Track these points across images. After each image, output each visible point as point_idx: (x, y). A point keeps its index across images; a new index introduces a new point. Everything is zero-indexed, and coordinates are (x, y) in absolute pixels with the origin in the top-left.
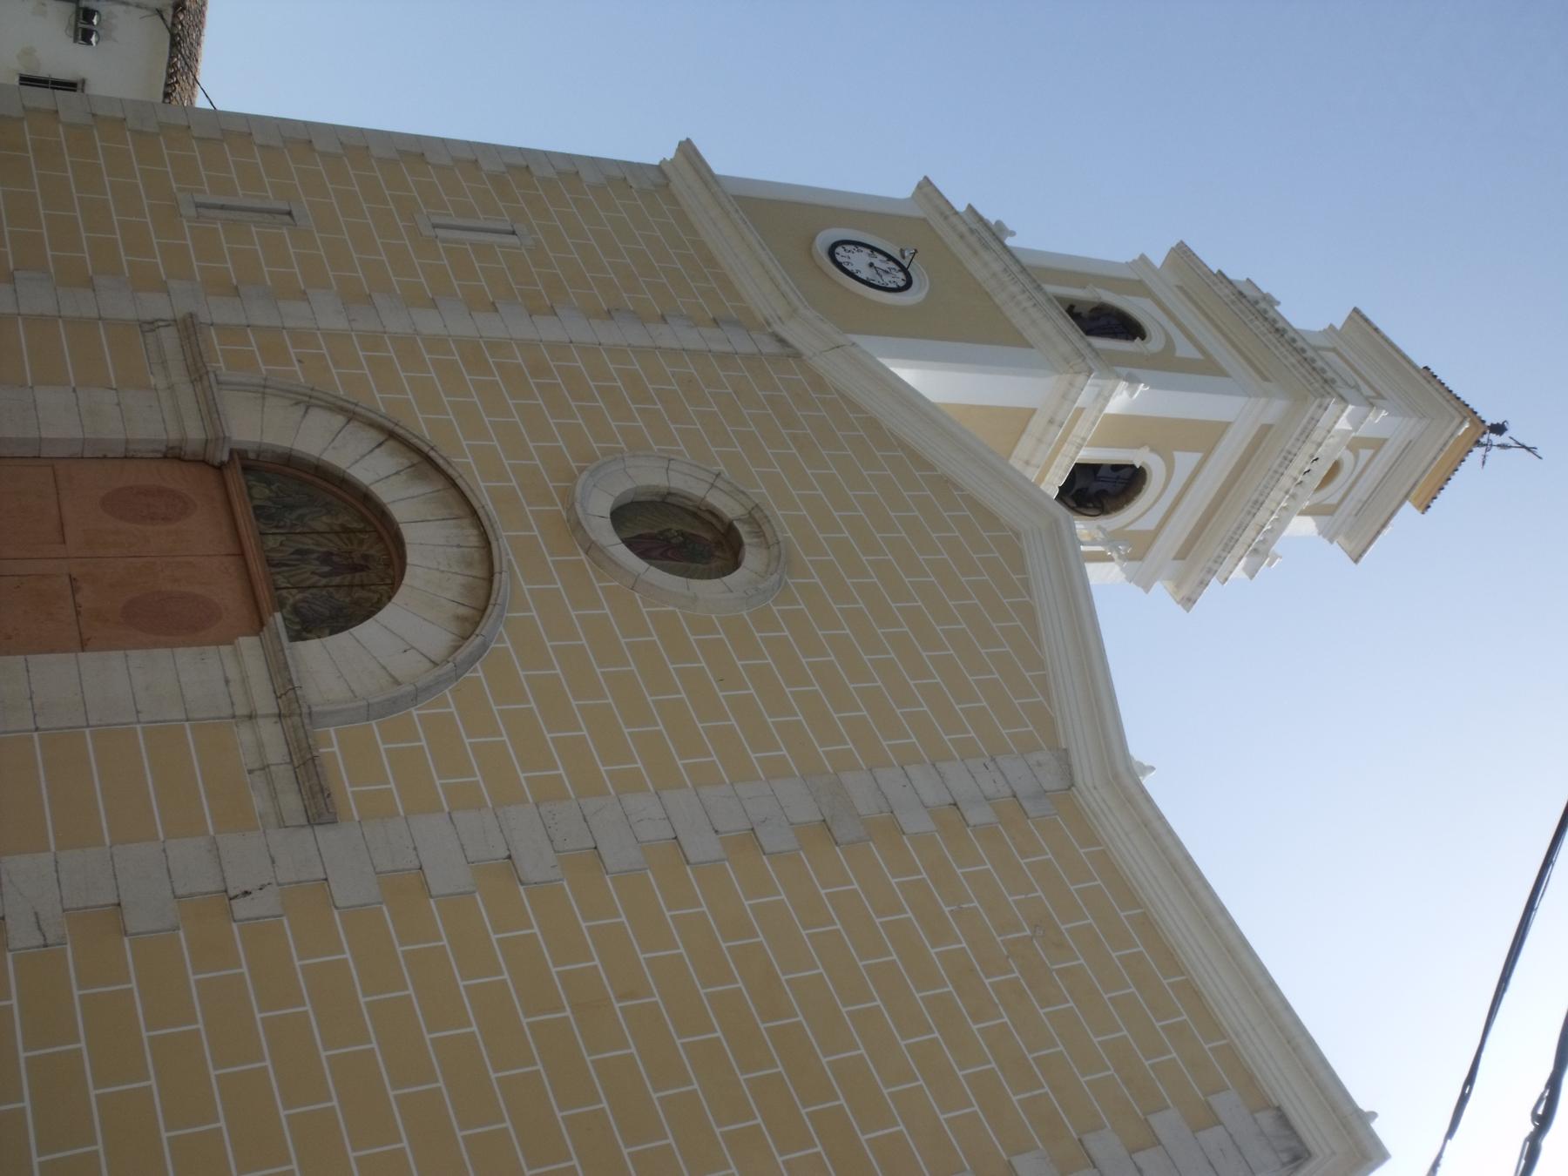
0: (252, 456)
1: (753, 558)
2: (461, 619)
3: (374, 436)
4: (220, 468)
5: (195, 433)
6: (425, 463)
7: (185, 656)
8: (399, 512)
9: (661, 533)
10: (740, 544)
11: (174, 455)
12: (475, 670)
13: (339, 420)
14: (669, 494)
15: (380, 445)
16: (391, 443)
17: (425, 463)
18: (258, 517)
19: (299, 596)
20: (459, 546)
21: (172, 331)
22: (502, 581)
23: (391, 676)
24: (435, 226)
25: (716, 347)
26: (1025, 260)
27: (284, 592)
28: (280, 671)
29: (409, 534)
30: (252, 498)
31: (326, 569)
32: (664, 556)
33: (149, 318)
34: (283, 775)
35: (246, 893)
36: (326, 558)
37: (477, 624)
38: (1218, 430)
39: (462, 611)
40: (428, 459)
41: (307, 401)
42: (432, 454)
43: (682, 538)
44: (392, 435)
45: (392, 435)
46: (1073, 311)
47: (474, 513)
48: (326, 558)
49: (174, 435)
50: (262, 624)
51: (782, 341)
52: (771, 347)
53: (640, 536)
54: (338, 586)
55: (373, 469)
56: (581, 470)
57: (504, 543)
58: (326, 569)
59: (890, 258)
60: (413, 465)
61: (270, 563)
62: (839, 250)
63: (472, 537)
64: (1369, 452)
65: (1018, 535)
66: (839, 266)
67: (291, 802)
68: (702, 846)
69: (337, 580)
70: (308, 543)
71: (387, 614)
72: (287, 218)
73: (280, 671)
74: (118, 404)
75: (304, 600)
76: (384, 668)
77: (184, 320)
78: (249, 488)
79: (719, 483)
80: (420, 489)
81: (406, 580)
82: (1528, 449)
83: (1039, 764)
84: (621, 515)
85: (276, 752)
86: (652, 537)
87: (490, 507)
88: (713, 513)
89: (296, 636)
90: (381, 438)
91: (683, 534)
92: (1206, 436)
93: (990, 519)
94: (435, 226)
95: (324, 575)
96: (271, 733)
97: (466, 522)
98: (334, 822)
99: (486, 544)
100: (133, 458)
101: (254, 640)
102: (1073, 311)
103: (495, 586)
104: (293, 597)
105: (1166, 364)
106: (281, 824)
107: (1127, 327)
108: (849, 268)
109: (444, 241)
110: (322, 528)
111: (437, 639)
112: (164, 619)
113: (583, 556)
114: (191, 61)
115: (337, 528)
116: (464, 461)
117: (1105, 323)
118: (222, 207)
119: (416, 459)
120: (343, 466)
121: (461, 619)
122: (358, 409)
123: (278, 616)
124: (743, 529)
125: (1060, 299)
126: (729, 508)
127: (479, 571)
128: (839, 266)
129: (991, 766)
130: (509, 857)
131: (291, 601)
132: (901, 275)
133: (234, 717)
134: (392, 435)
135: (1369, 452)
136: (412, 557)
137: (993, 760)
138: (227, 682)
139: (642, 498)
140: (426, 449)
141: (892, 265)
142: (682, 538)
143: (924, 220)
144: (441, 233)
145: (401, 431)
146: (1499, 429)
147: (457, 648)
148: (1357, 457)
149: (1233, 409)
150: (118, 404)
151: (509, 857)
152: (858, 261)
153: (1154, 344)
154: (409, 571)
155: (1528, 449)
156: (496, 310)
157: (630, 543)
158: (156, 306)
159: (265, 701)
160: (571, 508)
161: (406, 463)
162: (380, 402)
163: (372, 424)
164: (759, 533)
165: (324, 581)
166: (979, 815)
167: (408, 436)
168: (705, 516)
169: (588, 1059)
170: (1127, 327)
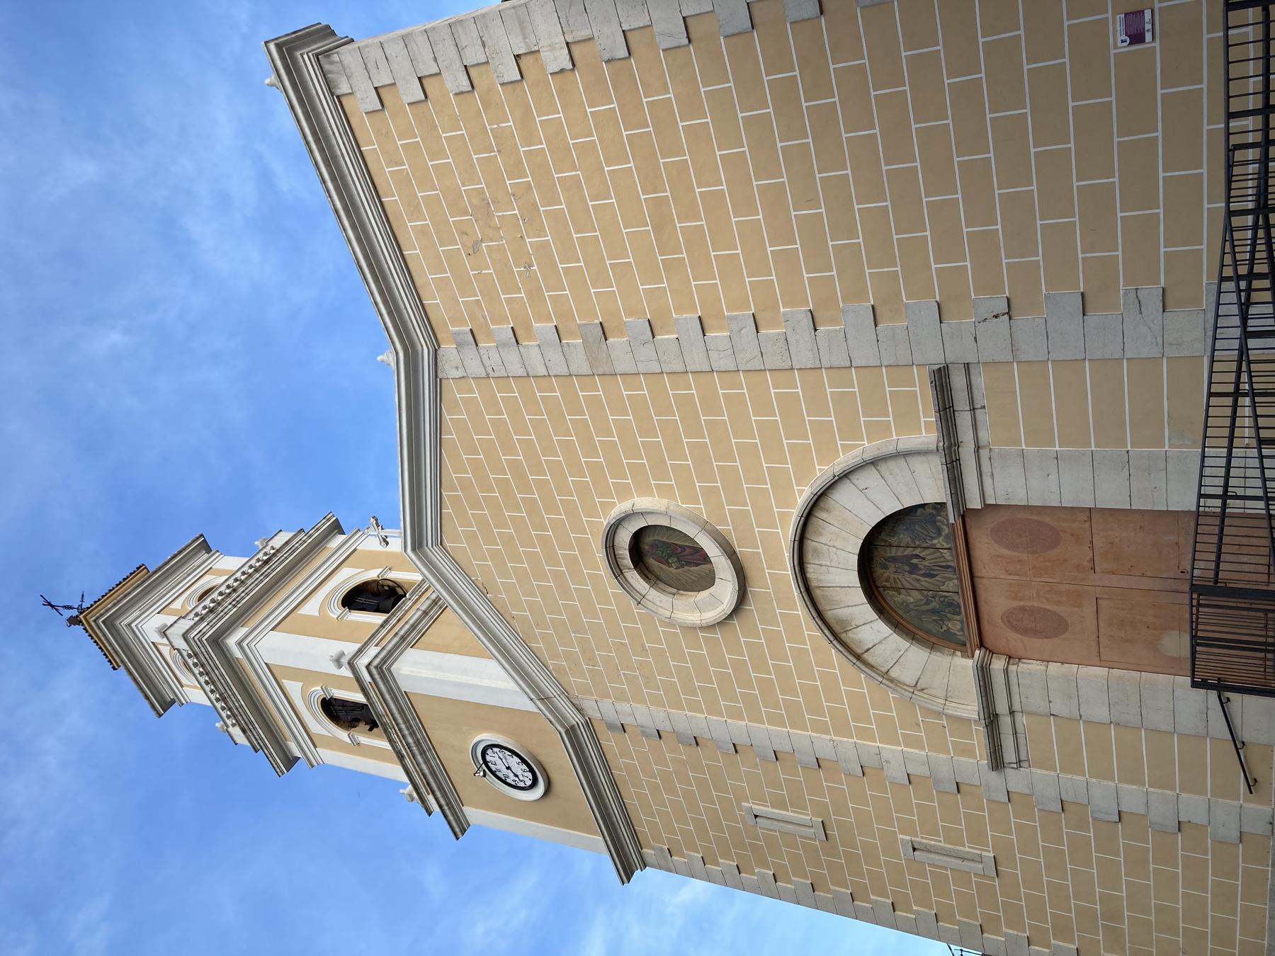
0: (959, 653)
2: (822, 515)
6: (835, 632)
7: (1019, 498)
8: (859, 596)
9: (683, 566)
13: (893, 674)
16: (859, 651)
17: (835, 632)
19: (935, 541)
31: (915, 561)
32: (683, 548)
35: (996, 317)
44: (858, 657)
45: (857, 656)
46: (352, 41)
53: (697, 565)
55: (871, 630)
57: (789, 566)
58: (915, 561)
59: (493, 773)
63: (811, 570)
67: (958, 381)
69: (908, 552)
70: (925, 582)
75: (933, 538)
80: (842, 613)
82: (50, 604)
83: (457, 368)
84: (708, 580)
86: (689, 564)
87: (796, 593)
90: (866, 656)
91: (669, 564)
95: (917, 556)
101: (970, 506)
104: (939, 542)
106: (967, 366)
110: (916, 594)
112: (1035, 528)
113: (737, 550)
115: (903, 591)
119: (843, 636)
123: (952, 521)
126: (634, 577)
127: (810, 545)
128: (532, 770)
132: (488, 758)
134: (857, 656)
141: (493, 767)
146: (74, 621)
153: (317, 692)
155: (50, 604)
157: (706, 559)
161: (850, 634)
162: (864, 684)
163: (872, 667)
165: (917, 552)
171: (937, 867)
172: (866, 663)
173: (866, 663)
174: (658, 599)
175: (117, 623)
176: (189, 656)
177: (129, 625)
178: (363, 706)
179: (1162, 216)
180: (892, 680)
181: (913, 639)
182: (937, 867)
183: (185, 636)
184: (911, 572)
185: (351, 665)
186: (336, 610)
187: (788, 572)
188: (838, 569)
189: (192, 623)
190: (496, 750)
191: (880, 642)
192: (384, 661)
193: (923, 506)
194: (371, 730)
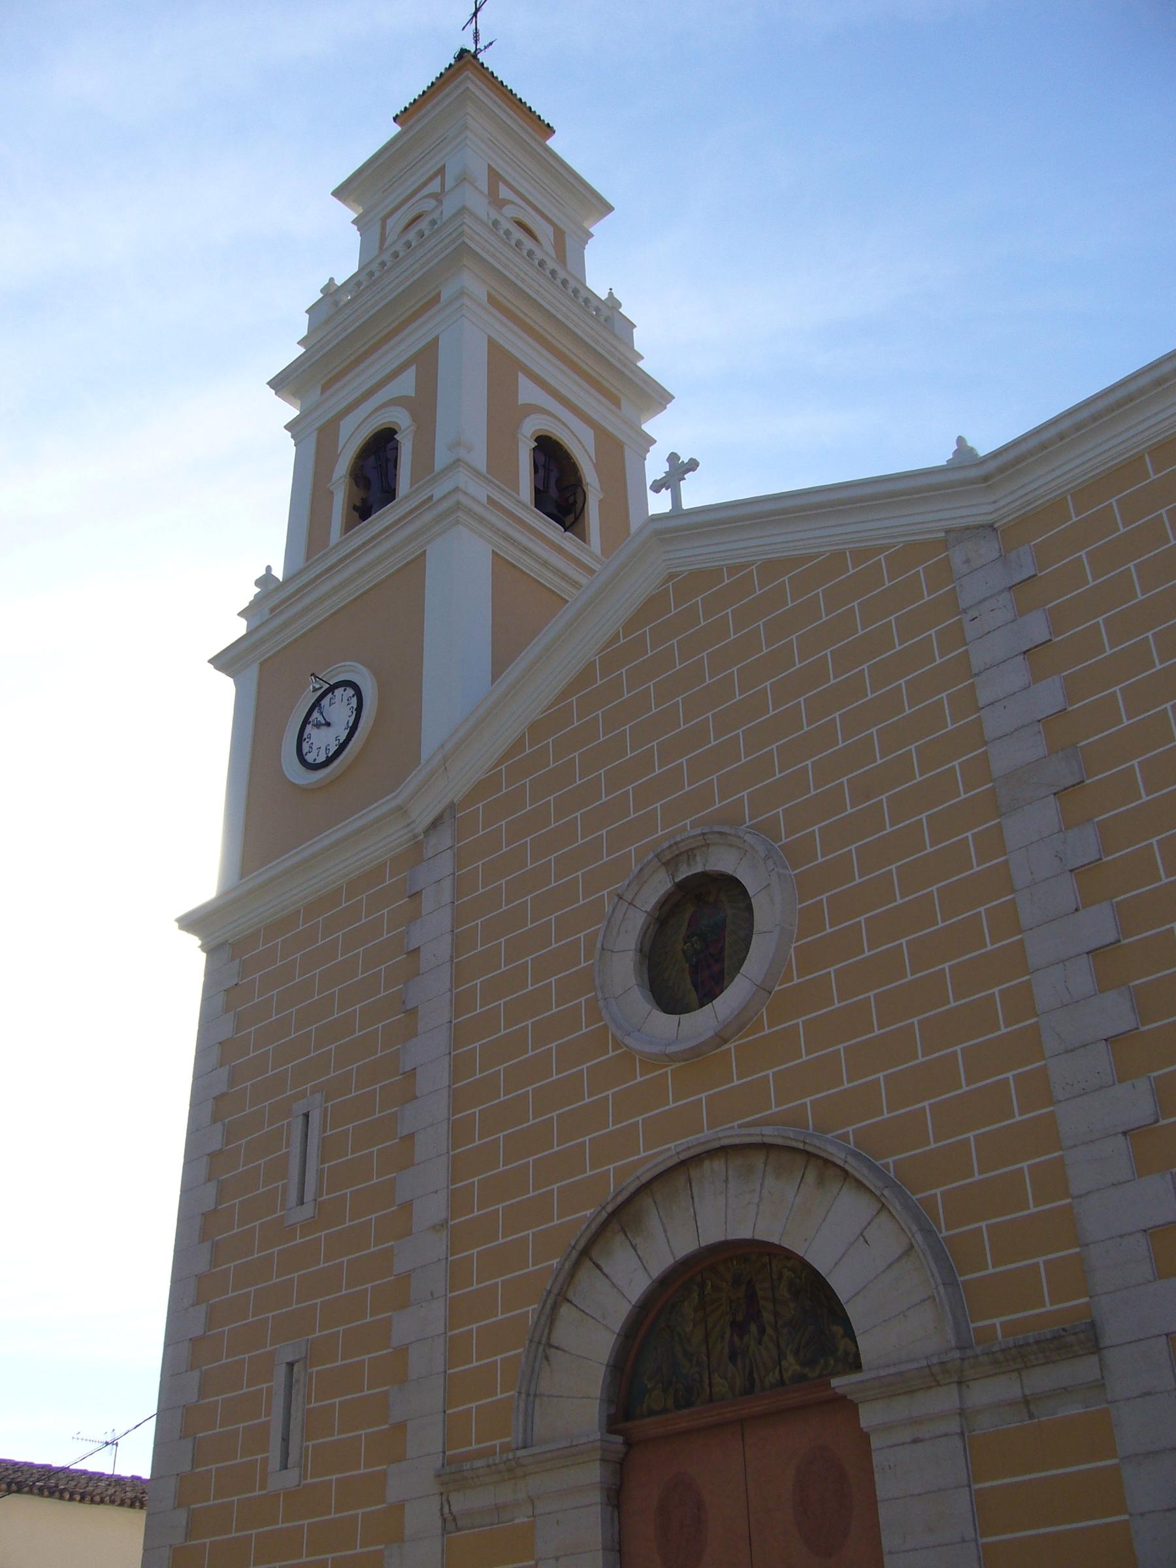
0: (612, 1411)
1: (723, 861)
2: (821, 1182)
3: (586, 1273)
4: (628, 1444)
5: (593, 1473)
6: (622, 1217)
7: (884, 1487)
8: (685, 1246)
10: (703, 875)
11: (616, 1497)
12: (886, 1166)
13: (565, 1309)
14: (641, 951)
15: (598, 1267)
16: (595, 1253)
17: (622, 1217)
18: (689, 1404)
19: (791, 1358)
20: (726, 1181)
21: (454, 1497)
22: (769, 1134)
23: (900, 1258)
24: (301, 1202)
25: (447, 897)
26: (301, 564)
27: (787, 1376)
28: (900, 1385)
29: (712, 1234)
30: (664, 1410)
31: (753, 1328)
33: (439, 1523)
34: (1041, 1379)
36: (739, 1328)
37: (827, 1162)
38: (495, 349)
39: (811, 1177)
40: (614, 1214)
41: (543, 1344)
42: (610, 1209)
43: (696, 938)
44: (585, 1253)
45: (587, 1253)
46: (362, 511)
47: (683, 1163)
48: (739, 1328)
49: (596, 1497)
50: (844, 1397)
51: (435, 824)
52: (444, 838)
54: (776, 1315)
55: (629, 1275)
56: (617, 1045)
58: (753, 1328)
60: (623, 1229)
61: (749, 1390)
62: (310, 758)
64: (502, 188)
65: (671, 576)
66: (329, 761)
67: (1085, 1369)
68: (1099, 925)
69: (767, 1316)
71: (821, 1265)
72: (296, 1368)
73: (900, 1385)
74: (557, 1558)
76: (890, 1266)
77: (442, 1484)
78: (652, 1413)
79: (628, 897)
80: (653, 1222)
81: (775, 1240)
82: (477, 10)
83: (967, 561)
85: (1005, 1388)
88: (663, 903)
89: (857, 1366)
90: (588, 1264)
92: (503, 368)
93: (653, 606)
94: (301, 1202)
95: (762, 1331)
96: (983, 1393)
97: (694, 1173)
98: (1093, 1324)
99: (724, 1151)
100: (620, 1543)
102: (362, 511)
103: (780, 1141)
104: (791, 1365)
105: (423, 405)
106: (1100, 1385)
107: (380, 453)
108: (333, 749)
109: (319, 1191)
111: (848, 1209)
114: (47, 1472)
116: (615, 1177)
117: (374, 476)
118: (286, 1440)
120: (630, 1308)
121: (821, 1182)
122: (555, 1291)
123: (834, 1382)
124: (684, 873)
125: (348, 527)
126: (659, 886)
127: (758, 1160)
128: (329, 761)
129: (973, 613)
130: (1125, 1133)
131: (798, 1368)
133: (962, 1434)
134: (587, 1253)
135: (502, 188)
136: (743, 1232)
137: (965, 611)
138: (915, 1441)
139: (646, 977)
140: (604, 1215)
142: (696, 938)
143: (261, 664)
144: (309, 1196)
145: (582, 1243)
147: (860, 1185)
148: (506, 202)
149: (466, 340)
150: (557, 1558)
151: (1125, 1133)
152: (322, 741)
153: (401, 419)
154: (760, 1236)
156: (411, 1136)
158: (423, 1516)
159: (944, 1399)
160: (672, 1058)
161: (620, 1237)
163: (572, 1275)
164: (689, 854)
166: (1036, 628)
167: (588, 1234)
168: (665, 915)
169: (900, 901)
170: (380, 453)
171: (325, 1122)
172: (577, 1264)
173: (577, 1264)
174: (633, 926)
175: (468, 73)
176: (433, 222)
177: (468, 78)
178: (629, 534)
179: (1026, 1212)
180: (555, 1308)
181: (626, 1336)
182: (325, 1122)
183: (463, 210)
184: (733, 1324)
185: (457, 462)
186: (531, 427)
187: (707, 1135)
188: (724, 1212)
189: (485, 218)
190: (354, 701)
191: (614, 1285)
192: (469, 512)
193: (850, 1333)
194: (355, 508)
